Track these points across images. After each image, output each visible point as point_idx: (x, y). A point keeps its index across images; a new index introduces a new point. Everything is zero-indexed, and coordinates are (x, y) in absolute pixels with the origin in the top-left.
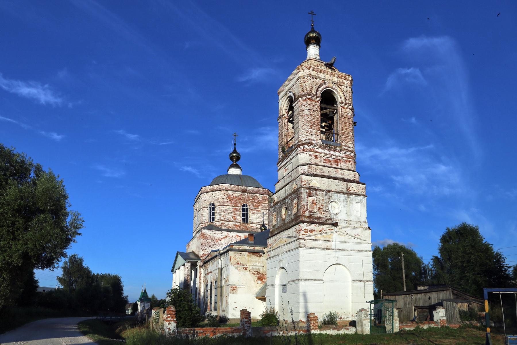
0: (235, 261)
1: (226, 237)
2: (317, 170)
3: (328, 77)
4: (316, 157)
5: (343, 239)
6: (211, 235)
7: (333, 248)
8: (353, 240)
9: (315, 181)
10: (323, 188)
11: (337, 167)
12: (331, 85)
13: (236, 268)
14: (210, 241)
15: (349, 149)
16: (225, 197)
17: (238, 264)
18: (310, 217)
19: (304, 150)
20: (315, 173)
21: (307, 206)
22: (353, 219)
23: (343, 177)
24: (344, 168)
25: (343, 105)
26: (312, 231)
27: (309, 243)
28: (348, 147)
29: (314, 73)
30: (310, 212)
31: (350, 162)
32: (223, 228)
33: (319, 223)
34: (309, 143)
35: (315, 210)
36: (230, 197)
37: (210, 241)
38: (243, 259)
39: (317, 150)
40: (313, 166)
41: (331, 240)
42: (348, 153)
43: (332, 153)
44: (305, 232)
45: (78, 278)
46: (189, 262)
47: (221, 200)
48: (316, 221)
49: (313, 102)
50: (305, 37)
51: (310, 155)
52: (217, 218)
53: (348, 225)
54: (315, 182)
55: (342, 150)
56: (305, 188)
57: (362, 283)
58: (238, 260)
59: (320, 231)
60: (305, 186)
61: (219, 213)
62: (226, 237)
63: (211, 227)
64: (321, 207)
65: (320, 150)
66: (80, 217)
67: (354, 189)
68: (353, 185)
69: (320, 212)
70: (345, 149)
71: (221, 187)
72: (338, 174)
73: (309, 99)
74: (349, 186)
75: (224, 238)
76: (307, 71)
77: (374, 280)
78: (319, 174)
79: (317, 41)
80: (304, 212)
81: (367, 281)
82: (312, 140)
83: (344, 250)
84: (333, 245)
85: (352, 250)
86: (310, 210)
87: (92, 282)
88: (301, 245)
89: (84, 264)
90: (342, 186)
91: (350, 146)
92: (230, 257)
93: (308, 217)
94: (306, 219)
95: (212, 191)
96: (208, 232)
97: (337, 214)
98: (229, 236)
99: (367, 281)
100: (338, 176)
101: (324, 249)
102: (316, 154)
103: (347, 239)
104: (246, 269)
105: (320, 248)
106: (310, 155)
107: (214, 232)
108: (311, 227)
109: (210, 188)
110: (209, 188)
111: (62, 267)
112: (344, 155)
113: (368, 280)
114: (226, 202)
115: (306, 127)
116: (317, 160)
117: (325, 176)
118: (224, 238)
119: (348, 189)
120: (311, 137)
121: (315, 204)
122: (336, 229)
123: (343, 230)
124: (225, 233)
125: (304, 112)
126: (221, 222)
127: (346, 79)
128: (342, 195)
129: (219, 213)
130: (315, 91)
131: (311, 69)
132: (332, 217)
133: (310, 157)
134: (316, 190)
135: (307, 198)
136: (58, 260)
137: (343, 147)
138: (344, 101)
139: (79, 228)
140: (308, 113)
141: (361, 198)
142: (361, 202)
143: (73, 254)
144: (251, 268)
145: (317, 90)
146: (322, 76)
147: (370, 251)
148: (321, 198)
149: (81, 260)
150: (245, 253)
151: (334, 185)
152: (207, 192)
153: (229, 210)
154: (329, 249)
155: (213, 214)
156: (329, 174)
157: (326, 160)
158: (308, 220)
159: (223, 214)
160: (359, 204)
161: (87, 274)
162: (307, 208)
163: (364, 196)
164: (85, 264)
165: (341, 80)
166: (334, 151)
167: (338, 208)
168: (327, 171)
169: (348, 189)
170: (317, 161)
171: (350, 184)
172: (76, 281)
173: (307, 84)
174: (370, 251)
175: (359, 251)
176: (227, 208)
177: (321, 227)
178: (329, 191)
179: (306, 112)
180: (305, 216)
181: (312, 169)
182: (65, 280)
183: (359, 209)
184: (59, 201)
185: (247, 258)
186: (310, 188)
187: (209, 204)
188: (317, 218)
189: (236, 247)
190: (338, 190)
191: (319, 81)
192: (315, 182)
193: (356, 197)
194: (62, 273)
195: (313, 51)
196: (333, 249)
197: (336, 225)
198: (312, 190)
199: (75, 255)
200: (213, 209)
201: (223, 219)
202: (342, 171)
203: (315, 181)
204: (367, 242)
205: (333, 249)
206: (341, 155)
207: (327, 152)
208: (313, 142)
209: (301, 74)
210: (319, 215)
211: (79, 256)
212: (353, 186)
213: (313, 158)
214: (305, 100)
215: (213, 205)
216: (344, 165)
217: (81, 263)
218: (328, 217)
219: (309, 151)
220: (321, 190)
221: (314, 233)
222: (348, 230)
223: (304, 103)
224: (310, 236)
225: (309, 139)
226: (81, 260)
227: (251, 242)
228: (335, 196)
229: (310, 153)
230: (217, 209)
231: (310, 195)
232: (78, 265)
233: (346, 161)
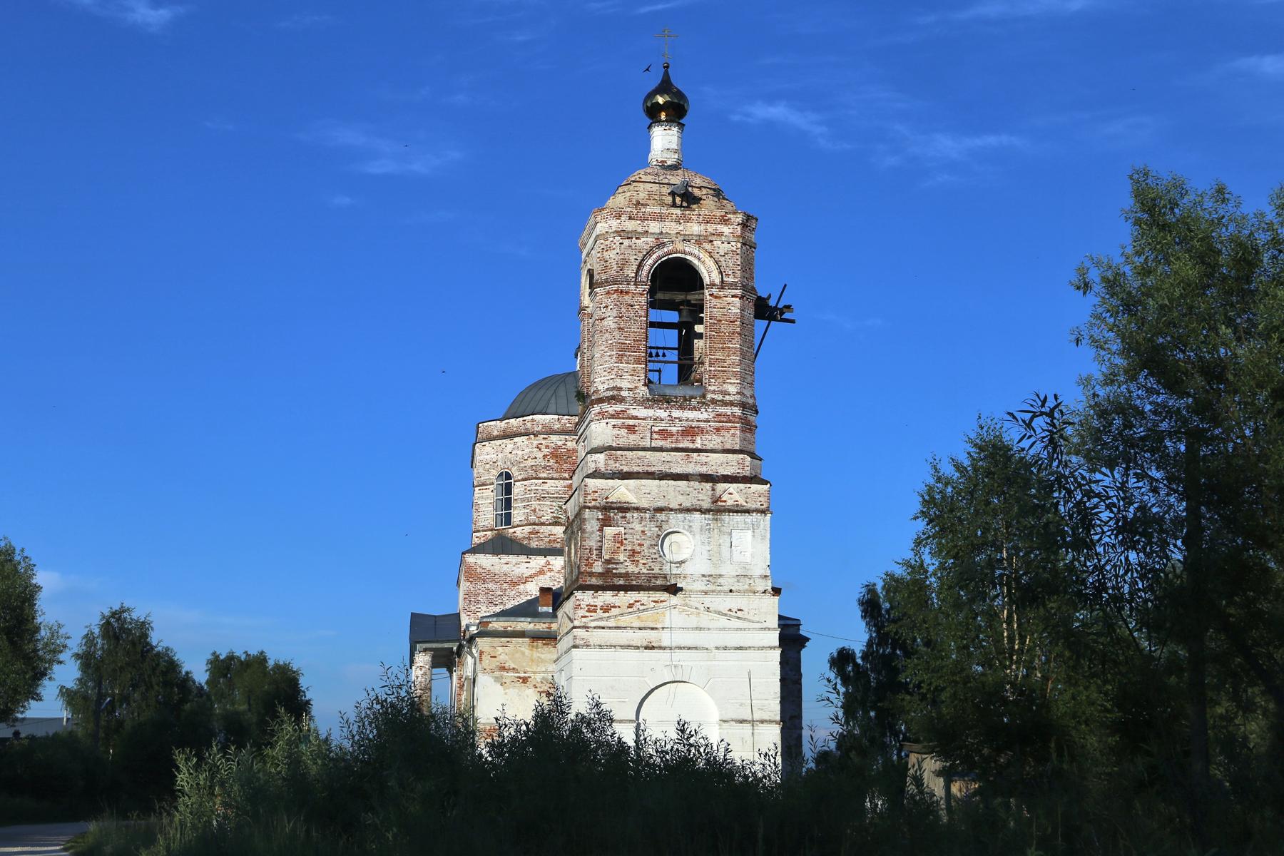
0: (495, 663)
1: (541, 572)
2: (630, 461)
3: (672, 227)
4: (631, 429)
5: (693, 621)
6: (496, 569)
7: (663, 644)
8: (723, 622)
9: (623, 489)
10: (644, 504)
11: (691, 446)
12: (680, 246)
13: (497, 679)
14: (491, 586)
15: (727, 398)
16: (540, 455)
17: (503, 668)
18: (607, 574)
19: (603, 415)
20: (626, 469)
21: (600, 549)
22: (728, 570)
23: (704, 470)
24: (710, 446)
25: (715, 291)
26: (606, 609)
27: (597, 637)
28: (725, 393)
29: (630, 225)
30: (608, 562)
31: (728, 429)
32: (534, 544)
33: (627, 588)
34: (613, 398)
35: (621, 557)
36: (556, 454)
37: (491, 586)
38: (517, 655)
39: (634, 413)
40: (619, 452)
41: (659, 626)
42: (722, 410)
43: (676, 414)
44: (589, 611)
45: (135, 686)
46: (425, 650)
47: (530, 462)
48: (621, 582)
49: (627, 298)
50: (645, 101)
51: (614, 427)
52: (518, 515)
53: (711, 587)
54: (624, 491)
55: (704, 404)
56: (595, 507)
57: (748, 727)
58: (503, 657)
59: (630, 606)
60: (593, 503)
61: (523, 500)
62: (541, 572)
63: (502, 545)
64: (638, 549)
65: (642, 412)
66: (62, 631)
67: (736, 496)
68: (733, 487)
69: (635, 562)
70: (714, 402)
71: (529, 425)
72: (692, 466)
73: (616, 291)
74: (718, 493)
75: (536, 575)
76: (614, 223)
77: (782, 719)
78: (636, 469)
79: (676, 112)
80: (590, 565)
81: (762, 722)
82: (620, 389)
83: (696, 648)
84: (665, 638)
85: (717, 648)
86: (607, 557)
87: (183, 701)
88: (578, 642)
89: (155, 638)
90: (702, 494)
91: (732, 389)
92: (481, 653)
93: (600, 575)
94: (594, 581)
95: (506, 435)
96: (485, 561)
97: (682, 562)
98: (550, 570)
99: (762, 722)
100: (690, 469)
101: (638, 648)
102: (631, 422)
103: (705, 620)
104: (525, 680)
105: (628, 647)
106: (614, 427)
107: (505, 558)
108: (608, 597)
109: (500, 425)
110: (496, 427)
111: (77, 656)
112: (712, 415)
113: (767, 718)
114: (546, 467)
115: (607, 359)
116: (632, 437)
117: (652, 473)
118: (536, 575)
119: (716, 500)
120: (618, 383)
121: (622, 543)
122: (674, 600)
123: (695, 600)
124: (538, 561)
125: (605, 323)
126: (528, 529)
127: (725, 221)
128: (697, 516)
129: (523, 500)
130: (635, 268)
131: (623, 218)
132: (666, 569)
133: (616, 432)
134: (624, 509)
135: (601, 530)
136: (24, 707)
137: (709, 396)
138: (717, 281)
139: (61, 652)
140: (613, 326)
141: (755, 517)
142: (754, 527)
143: (116, 607)
144: (539, 677)
145: (640, 266)
146: (654, 227)
147: (774, 648)
148: (638, 527)
149: (144, 627)
150: (520, 640)
151: (673, 493)
152: (490, 438)
153: (552, 490)
154: (653, 648)
155: (508, 504)
156: (665, 469)
157: (661, 432)
158: (600, 582)
159: (535, 503)
160: (750, 532)
161: (164, 674)
162: (600, 556)
163: (763, 512)
164: (158, 639)
165: (711, 228)
166: (682, 408)
167: (688, 547)
168: (657, 461)
169: (716, 500)
170: (633, 439)
171: (721, 487)
172: (125, 699)
173: (612, 254)
174: (774, 648)
175: (740, 648)
176: (546, 487)
177: (632, 596)
178: (660, 510)
179: (610, 323)
180: (591, 574)
181: (616, 460)
182: (85, 698)
183: (749, 545)
184: (22, 609)
185: (527, 652)
186: (607, 508)
187: (495, 473)
188: (626, 575)
189: (497, 625)
190: (687, 504)
191: (644, 243)
192: (624, 491)
193: (739, 518)
194: (78, 674)
195: (664, 140)
196: (664, 648)
197: (674, 590)
198: (612, 511)
199: (122, 611)
200: (508, 490)
201: (533, 518)
202: (703, 457)
203: (623, 489)
204: (765, 625)
205: (664, 648)
206: (704, 416)
207: (662, 414)
208: (624, 394)
209: (601, 228)
210: (632, 569)
211: (138, 614)
212: (731, 490)
213: (624, 432)
214: (608, 293)
215: (508, 476)
216: (713, 441)
217: (145, 636)
218: (656, 571)
219: (613, 417)
220: (637, 509)
221: (614, 612)
222: (709, 601)
223: (606, 301)
224: (601, 619)
225: (614, 388)
226: (143, 628)
227: (544, 609)
228: (675, 521)
229: (613, 422)
230: (517, 489)
231: (606, 522)
232: (133, 643)
233: (718, 430)
